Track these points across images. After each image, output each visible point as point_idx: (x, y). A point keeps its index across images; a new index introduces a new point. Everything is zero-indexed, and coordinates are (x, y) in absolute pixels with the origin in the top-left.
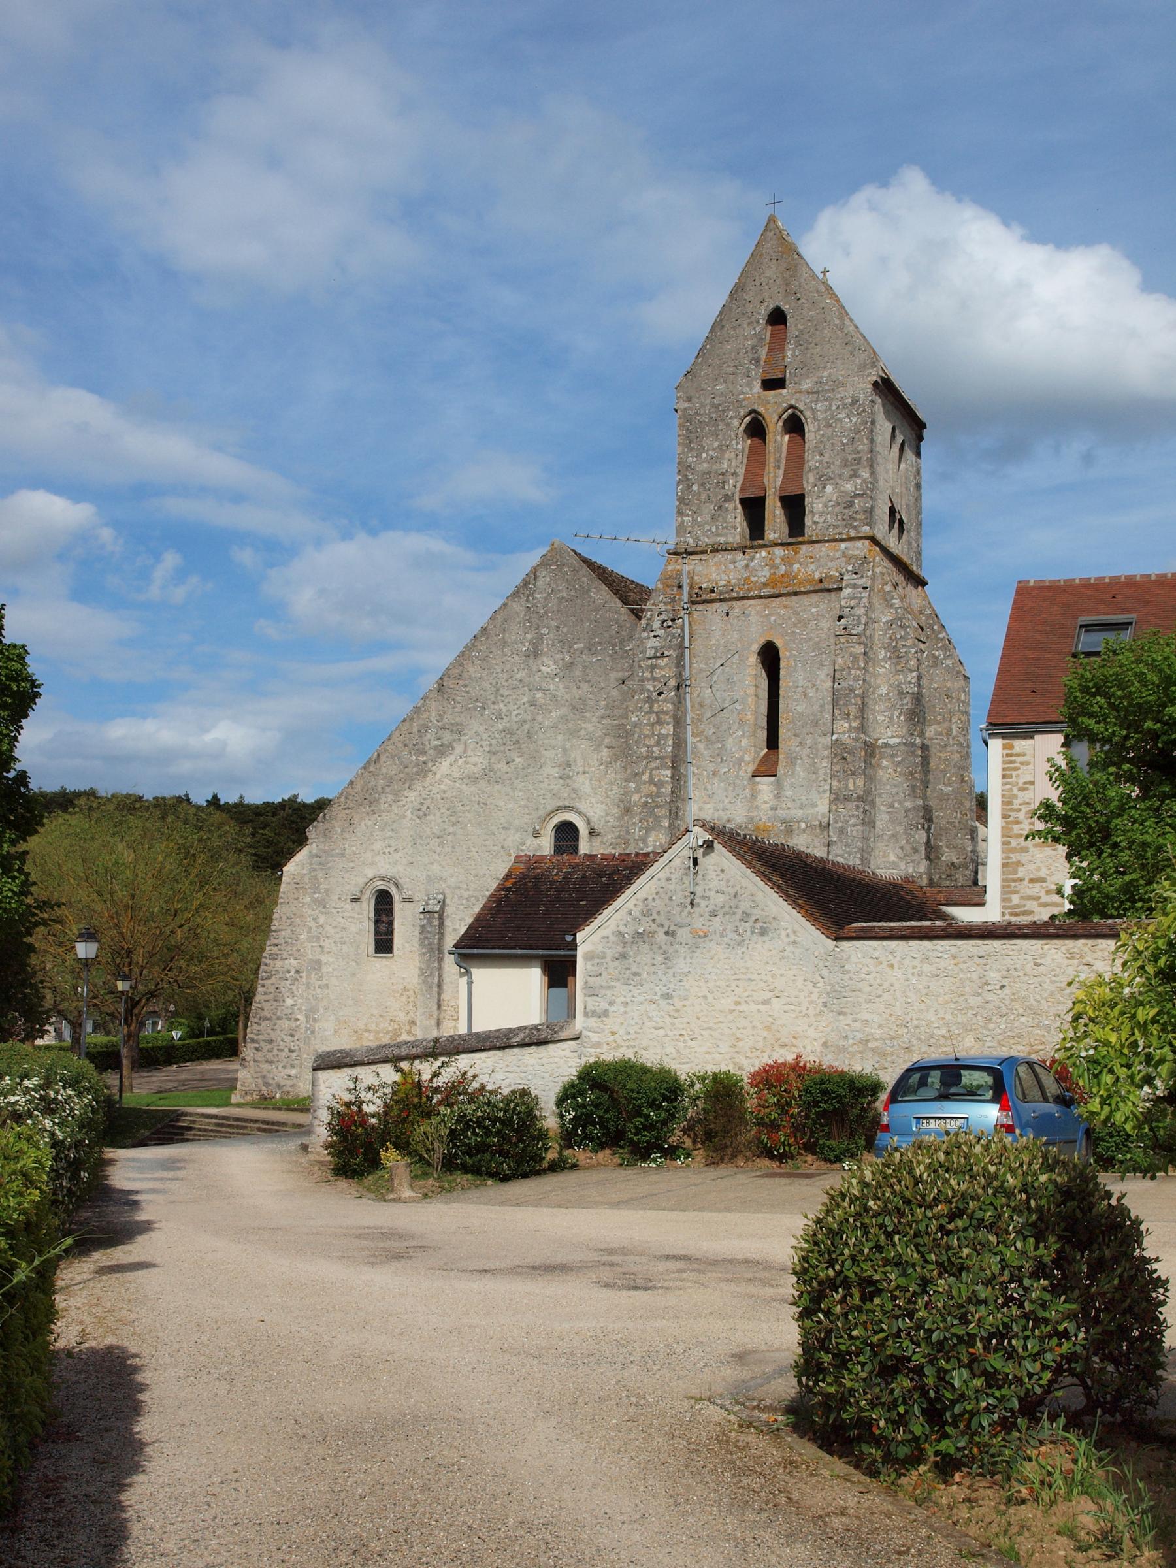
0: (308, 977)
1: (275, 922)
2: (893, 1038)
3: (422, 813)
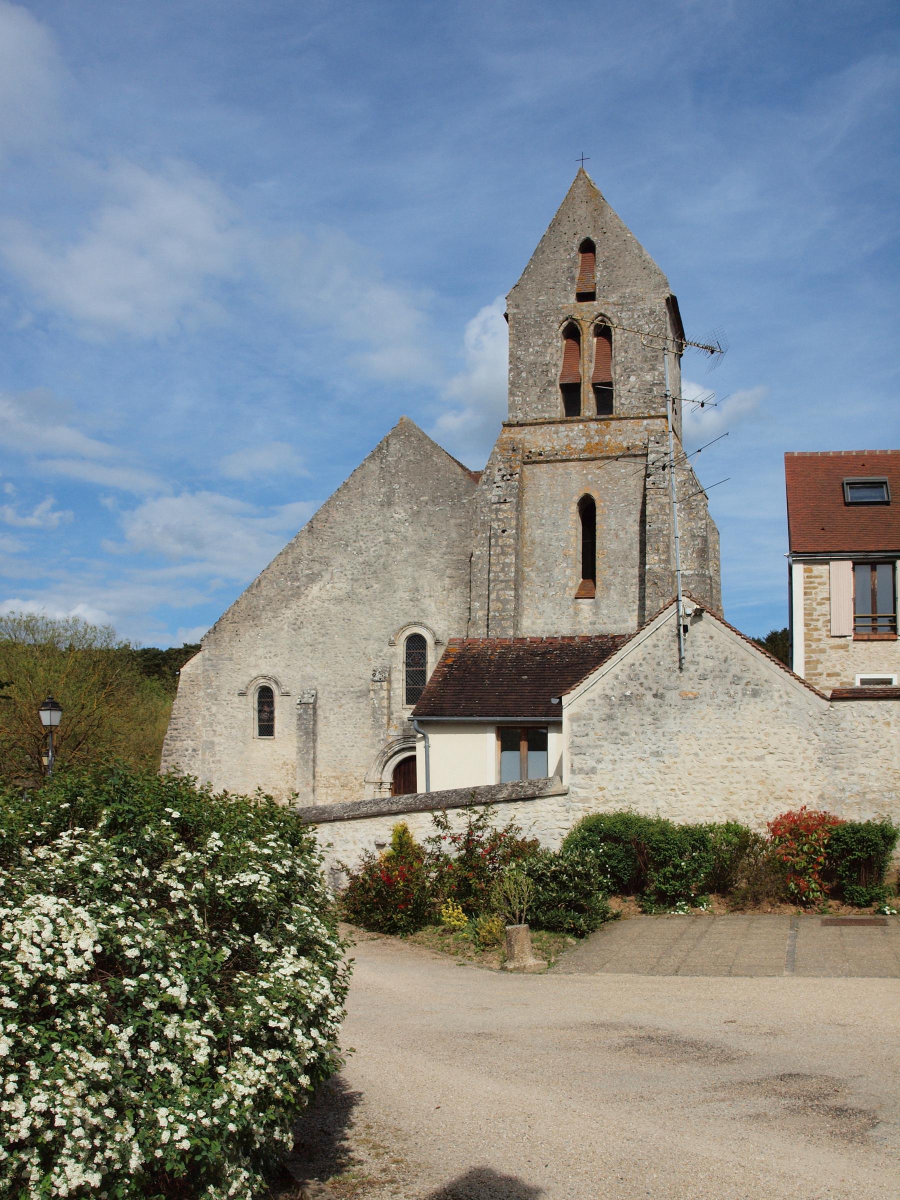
0: (204, 754)
1: (175, 712)
2: (890, 790)
3: (297, 626)
